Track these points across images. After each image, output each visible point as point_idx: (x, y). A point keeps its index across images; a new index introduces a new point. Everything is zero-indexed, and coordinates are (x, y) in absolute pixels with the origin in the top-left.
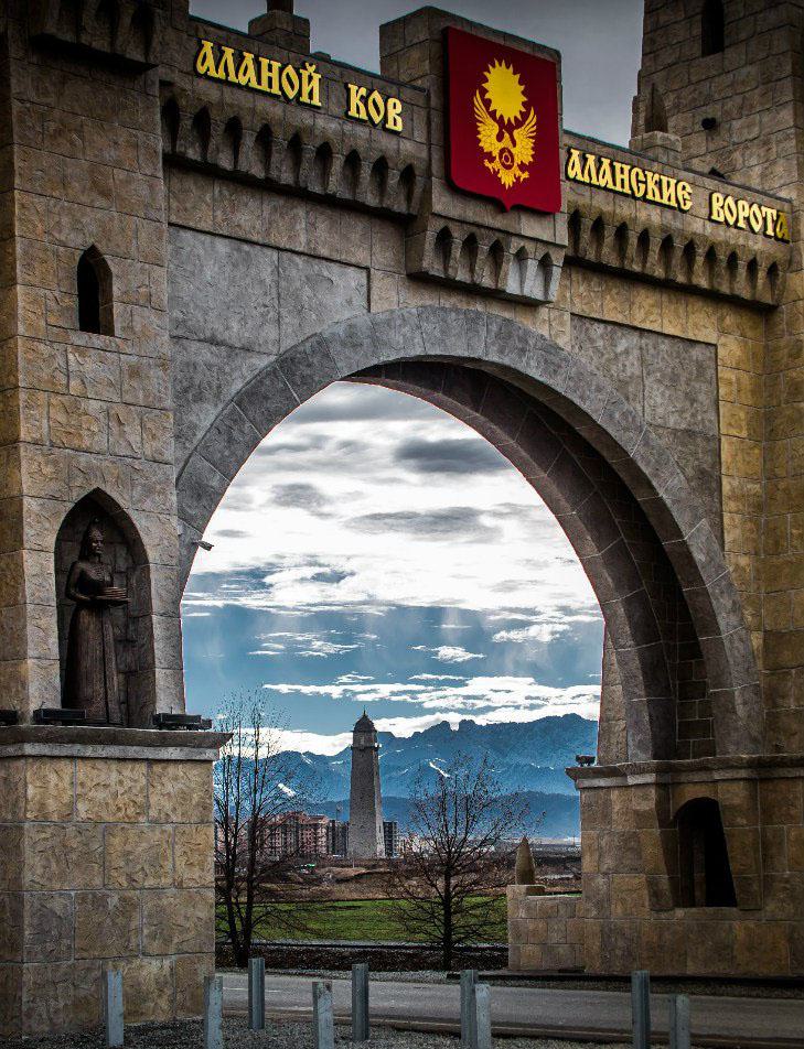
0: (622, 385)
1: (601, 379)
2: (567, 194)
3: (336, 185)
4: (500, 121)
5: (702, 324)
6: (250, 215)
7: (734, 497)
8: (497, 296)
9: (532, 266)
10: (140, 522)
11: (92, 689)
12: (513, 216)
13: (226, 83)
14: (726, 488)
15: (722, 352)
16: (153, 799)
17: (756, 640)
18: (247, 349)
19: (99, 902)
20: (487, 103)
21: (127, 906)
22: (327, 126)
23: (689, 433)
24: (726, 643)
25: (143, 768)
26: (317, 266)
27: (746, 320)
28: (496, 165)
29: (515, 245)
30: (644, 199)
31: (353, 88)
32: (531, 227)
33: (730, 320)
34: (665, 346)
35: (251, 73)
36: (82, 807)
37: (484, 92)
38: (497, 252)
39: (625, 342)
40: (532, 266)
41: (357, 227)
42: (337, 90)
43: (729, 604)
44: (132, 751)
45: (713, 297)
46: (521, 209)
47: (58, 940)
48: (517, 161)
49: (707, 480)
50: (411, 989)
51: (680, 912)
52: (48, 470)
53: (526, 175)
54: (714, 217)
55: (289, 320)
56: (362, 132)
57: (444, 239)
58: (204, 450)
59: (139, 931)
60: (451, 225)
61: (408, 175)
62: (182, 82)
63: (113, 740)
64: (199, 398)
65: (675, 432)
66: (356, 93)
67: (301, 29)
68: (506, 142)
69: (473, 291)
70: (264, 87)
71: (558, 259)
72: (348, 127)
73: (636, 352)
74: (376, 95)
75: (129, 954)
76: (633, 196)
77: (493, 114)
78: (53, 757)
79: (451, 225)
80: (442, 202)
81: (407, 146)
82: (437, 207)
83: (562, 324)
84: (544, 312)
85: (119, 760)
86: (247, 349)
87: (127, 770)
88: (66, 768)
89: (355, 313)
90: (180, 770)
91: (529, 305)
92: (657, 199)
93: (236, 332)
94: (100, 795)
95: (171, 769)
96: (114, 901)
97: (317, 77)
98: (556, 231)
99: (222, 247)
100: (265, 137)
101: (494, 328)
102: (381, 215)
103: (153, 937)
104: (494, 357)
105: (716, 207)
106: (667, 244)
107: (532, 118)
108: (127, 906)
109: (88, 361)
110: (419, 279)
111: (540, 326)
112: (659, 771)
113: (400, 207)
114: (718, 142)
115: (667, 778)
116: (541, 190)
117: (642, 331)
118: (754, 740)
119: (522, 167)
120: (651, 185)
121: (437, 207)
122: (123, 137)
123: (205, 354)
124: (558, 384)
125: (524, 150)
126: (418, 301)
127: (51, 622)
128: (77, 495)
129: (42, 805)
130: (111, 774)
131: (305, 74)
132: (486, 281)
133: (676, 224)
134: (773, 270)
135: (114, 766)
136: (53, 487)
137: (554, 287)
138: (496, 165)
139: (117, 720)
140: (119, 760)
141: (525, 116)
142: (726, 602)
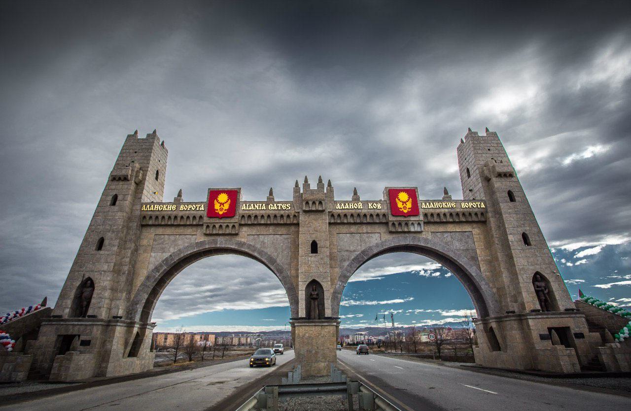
0: (446, 243)
1: (440, 243)
2: (421, 211)
3: (368, 220)
4: (403, 202)
5: (467, 228)
6: (353, 229)
7: (482, 260)
8: (409, 232)
9: (416, 225)
10: (322, 284)
11: (312, 314)
12: (409, 217)
13: (343, 209)
14: (479, 259)
15: (473, 232)
16: (322, 333)
17: (495, 290)
18: (354, 251)
19: (311, 352)
20: (399, 200)
21: (317, 353)
22: (364, 211)
23: (467, 250)
24: (485, 292)
25: (320, 327)
26: (369, 235)
27: (479, 225)
28: (403, 209)
29: (410, 223)
30: (443, 208)
31: (369, 204)
32: (412, 219)
33: (475, 226)
34: (457, 234)
35: (432, 206)
36: (307, 335)
37: (217, 199)
38: (407, 224)
39: (446, 235)
40: (416, 225)
41: (376, 227)
42: (366, 205)
43: (484, 283)
44: (317, 324)
45: (467, 222)
46: (408, 216)
47: (302, 359)
48: (408, 208)
49: (474, 258)
50: (185, 376)
51: (494, 352)
52: (304, 277)
53: (410, 210)
54: (462, 207)
55: (363, 245)
56: (373, 210)
57: (393, 224)
58: (346, 270)
59: (319, 357)
60: (420, 222)
61: (384, 215)
62: (334, 211)
63: (312, 322)
64: (345, 261)
65: (463, 250)
66: (370, 205)
67: (450, 197)
68: (405, 205)
69: (404, 232)
70: (350, 208)
71: (422, 223)
72: (369, 210)
73: (450, 236)
74: (374, 204)
75: (317, 361)
76: (439, 208)
77: (401, 201)
78: (301, 326)
79: (215, 224)
80: (391, 218)
81: (383, 211)
82: (390, 219)
83: (429, 234)
84: (424, 233)
85: (315, 326)
86: (354, 251)
87: (317, 327)
88: (303, 327)
89: (379, 241)
90: (328, 327)
91: (420, 232)
92: (446, 207)
93: (352, 248)
94: (311, 332)
95: (326, 327)
96: (314, 352)
97: (361, 204)
98: (421, 217)
99: (348, 235)
100: (476, 214)
101: (411, 238)
102: (381, 223)
103: (322, 358)
104: (411, 243)
105: (462, 205)
106: (451, 215)
107: (411, 200)
108: (317, 353)
109: (313, 258)
110: (391, 232)
111: (423, 235)
112: (482, 320)
113: (384, 221)
114: (473, 193)
115: (485, 322)
116: (415, 211)
117: (451, 232)
118: (497, 312)
119: (409, 209)
120: (444, 205)
121: (390, 219)
122: (320, 222)
123: (346, 253)
124: (429, 246)
125: (409, 205)
126: (390, 237)
127: (304, 302)
128: (310, 280)
129: (299, 334)
130: (313, 328)
131: (359, 204)
132: (406, 230)
133: (452, 211)
134: (482, 214)
135: (314, 327)
136: (305, 280)
137: (423, 228)
138: (403, 209)
139: (317, 318)
140: (315, 326)
141: (408, 200)
142: (483, 283)
